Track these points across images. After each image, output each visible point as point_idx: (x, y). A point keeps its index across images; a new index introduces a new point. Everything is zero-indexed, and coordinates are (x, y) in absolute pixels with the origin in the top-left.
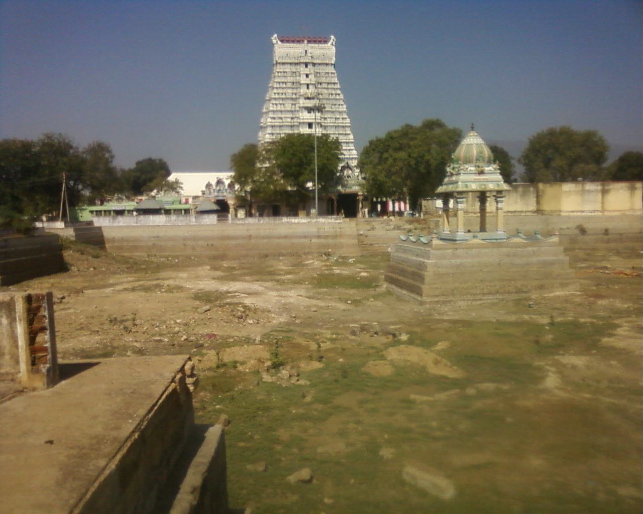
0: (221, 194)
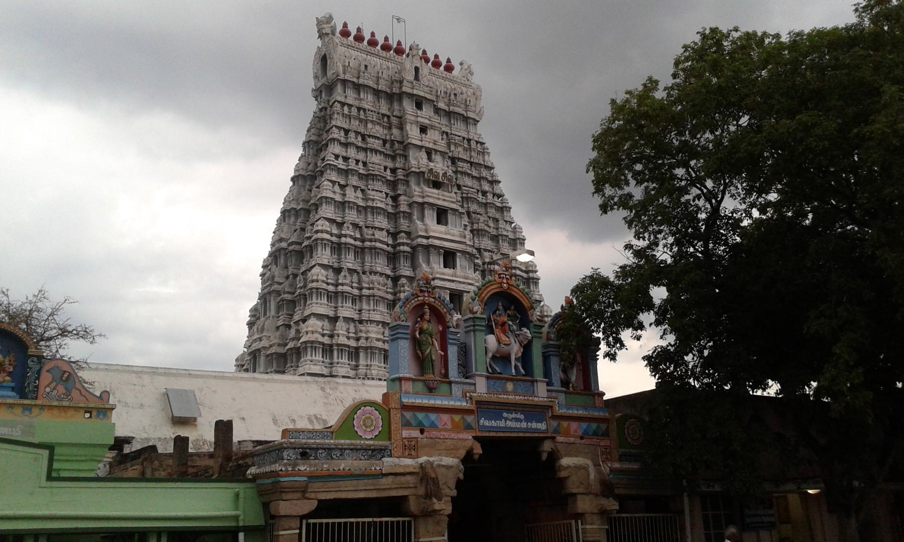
0: (511, 393)
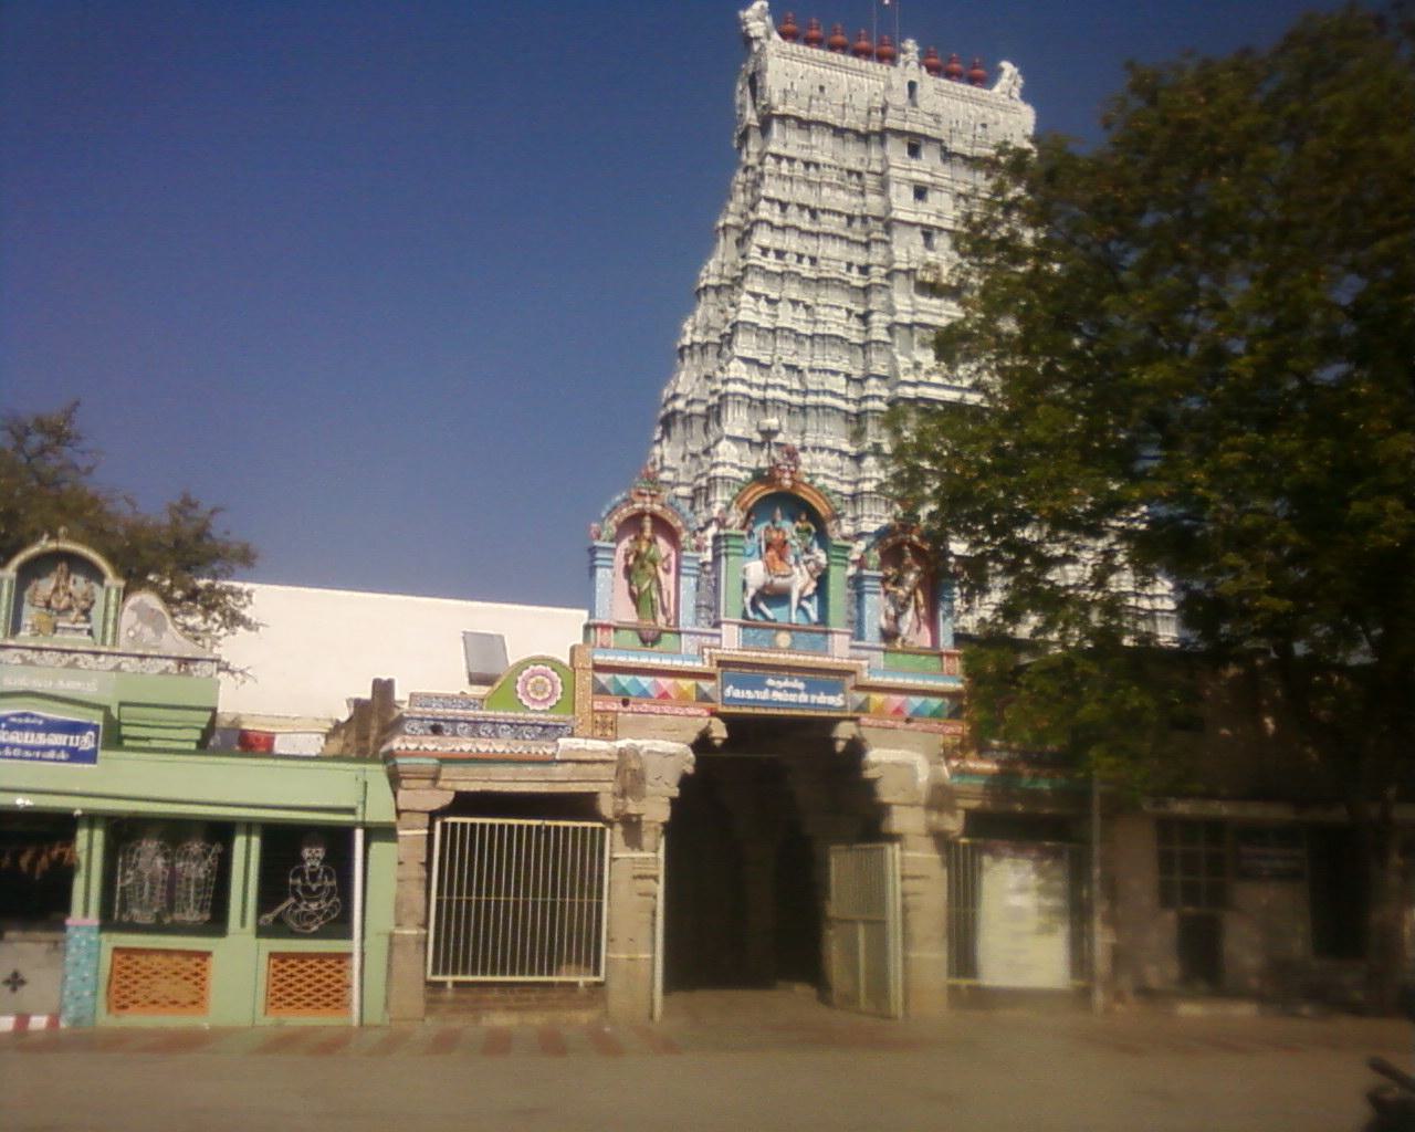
0: (783, 649)
